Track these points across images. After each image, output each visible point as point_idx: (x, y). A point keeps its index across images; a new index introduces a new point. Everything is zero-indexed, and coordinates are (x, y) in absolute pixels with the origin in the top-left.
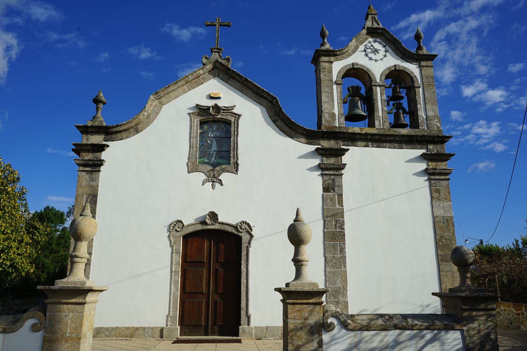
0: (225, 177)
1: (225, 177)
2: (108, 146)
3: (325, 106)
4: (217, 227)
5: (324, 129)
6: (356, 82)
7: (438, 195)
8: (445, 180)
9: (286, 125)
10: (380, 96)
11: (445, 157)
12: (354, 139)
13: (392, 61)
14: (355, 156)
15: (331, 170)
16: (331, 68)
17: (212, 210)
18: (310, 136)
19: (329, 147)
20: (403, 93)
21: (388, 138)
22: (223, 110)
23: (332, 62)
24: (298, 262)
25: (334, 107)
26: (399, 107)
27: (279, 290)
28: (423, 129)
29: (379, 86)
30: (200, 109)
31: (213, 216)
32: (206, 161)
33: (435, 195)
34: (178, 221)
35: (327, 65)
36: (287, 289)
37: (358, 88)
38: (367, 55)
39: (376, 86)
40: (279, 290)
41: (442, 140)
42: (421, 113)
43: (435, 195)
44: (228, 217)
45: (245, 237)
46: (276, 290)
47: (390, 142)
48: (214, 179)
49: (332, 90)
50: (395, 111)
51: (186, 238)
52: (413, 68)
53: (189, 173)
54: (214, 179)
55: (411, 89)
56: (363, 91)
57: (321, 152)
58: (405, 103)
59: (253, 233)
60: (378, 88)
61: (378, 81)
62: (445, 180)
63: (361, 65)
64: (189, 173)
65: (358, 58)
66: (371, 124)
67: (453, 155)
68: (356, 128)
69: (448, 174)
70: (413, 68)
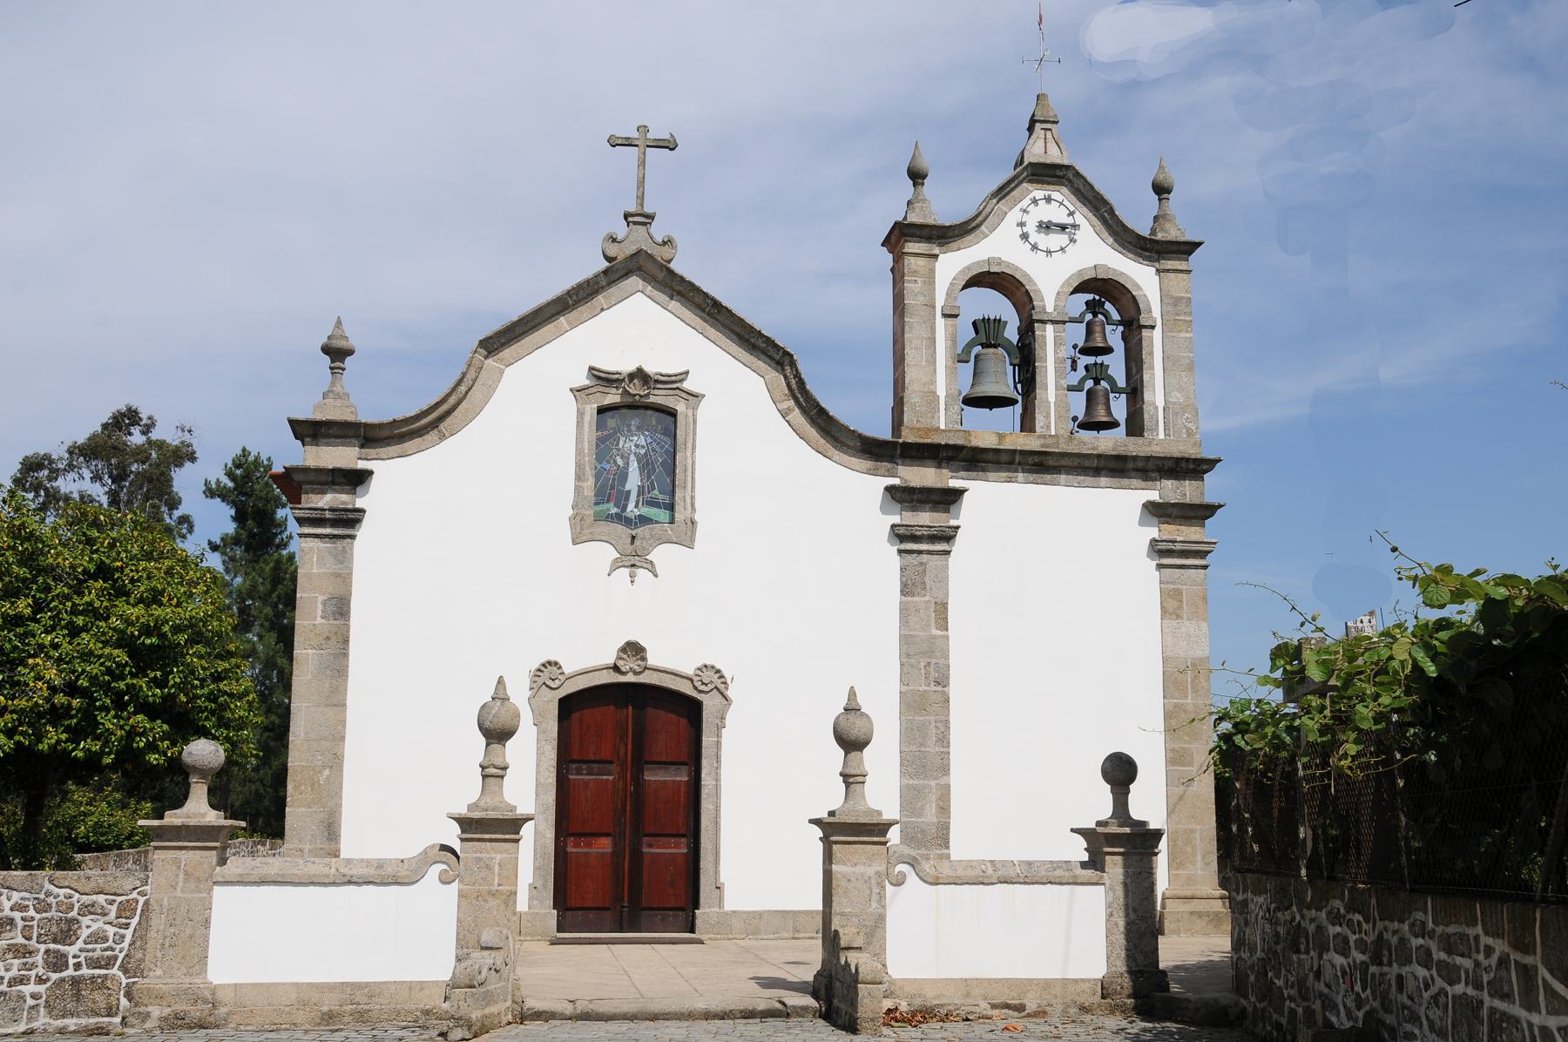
0: (662, 555)
1: (662, 555)
2: (370, 473)
3: (912, 374)
4: (646, 678)
5: (908, 437)
6: (995, 305)
7: (1176, 604)
8: (1196, 567)
9: (813, 422)
10: (1053, 348)
11: (1200, 513)
12: (975, 460)
13: (1094, 252)
14: (985, 498)
15: (924, 520)
16: (932, 271)
17: (633, 638)
18: (876, 451)
19: (923, 475)
20: (1114, 337)
21: (1065, 462)
22: (657, 381)
23: (936, 256)
24: (851, 779)
25: (939, 380)
26: (1097, 374)
27: (816, 822)
28: (1160, 439)
29: (1054, 322)
30: (599, 378)
31: (634, 649)
32: (614, 510)
33: (1172, 604)
34: (549, 663)
35: (921, 262)
36: (832, 820)
37: (999, 323)
38: (1025, 236)
39: (1043, 322)
40: (816, 822)
41: (1192, 468)
42: (1156, 395)
43: (1172, 604)
44: (673, 657)
45: (710, 703)
46: (811, 821)
47: (1071, 470)
48: (634, 560)
49: (933, 329)
50: (1089, 384)
51: (569, 706)
52: (1142, 277)
53: (575, 543)
54: (634, 560)
55: (1133, 326)
56: (1012, 334)
57: (901, 496)
58: (1116, 365)
59: (729, 693)
60: (1049, 327)
61: (1050, 308)
62: (1196, 567)
63: (1009, 265)
64: (575, 543)
65: (999, 245)
66: (1027, 423)
67: (1220, 506)
68: (990, 429)
69: (1203, 554)
70: (1142, 277)
